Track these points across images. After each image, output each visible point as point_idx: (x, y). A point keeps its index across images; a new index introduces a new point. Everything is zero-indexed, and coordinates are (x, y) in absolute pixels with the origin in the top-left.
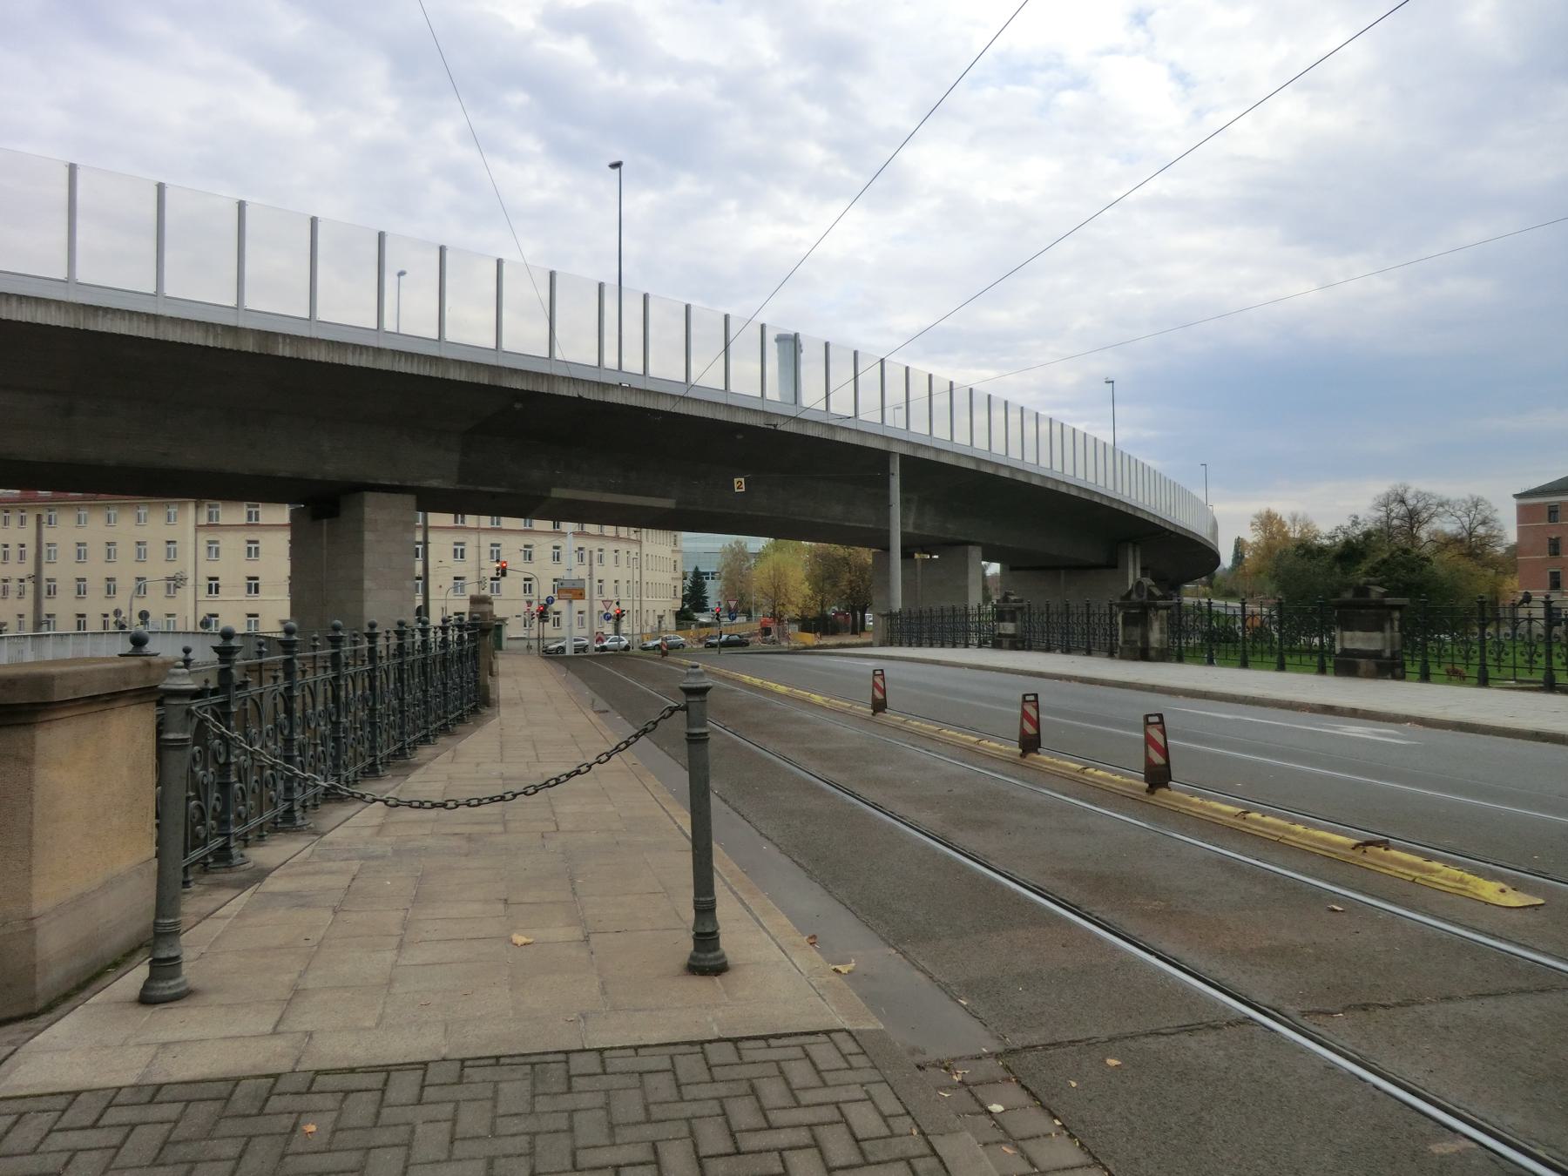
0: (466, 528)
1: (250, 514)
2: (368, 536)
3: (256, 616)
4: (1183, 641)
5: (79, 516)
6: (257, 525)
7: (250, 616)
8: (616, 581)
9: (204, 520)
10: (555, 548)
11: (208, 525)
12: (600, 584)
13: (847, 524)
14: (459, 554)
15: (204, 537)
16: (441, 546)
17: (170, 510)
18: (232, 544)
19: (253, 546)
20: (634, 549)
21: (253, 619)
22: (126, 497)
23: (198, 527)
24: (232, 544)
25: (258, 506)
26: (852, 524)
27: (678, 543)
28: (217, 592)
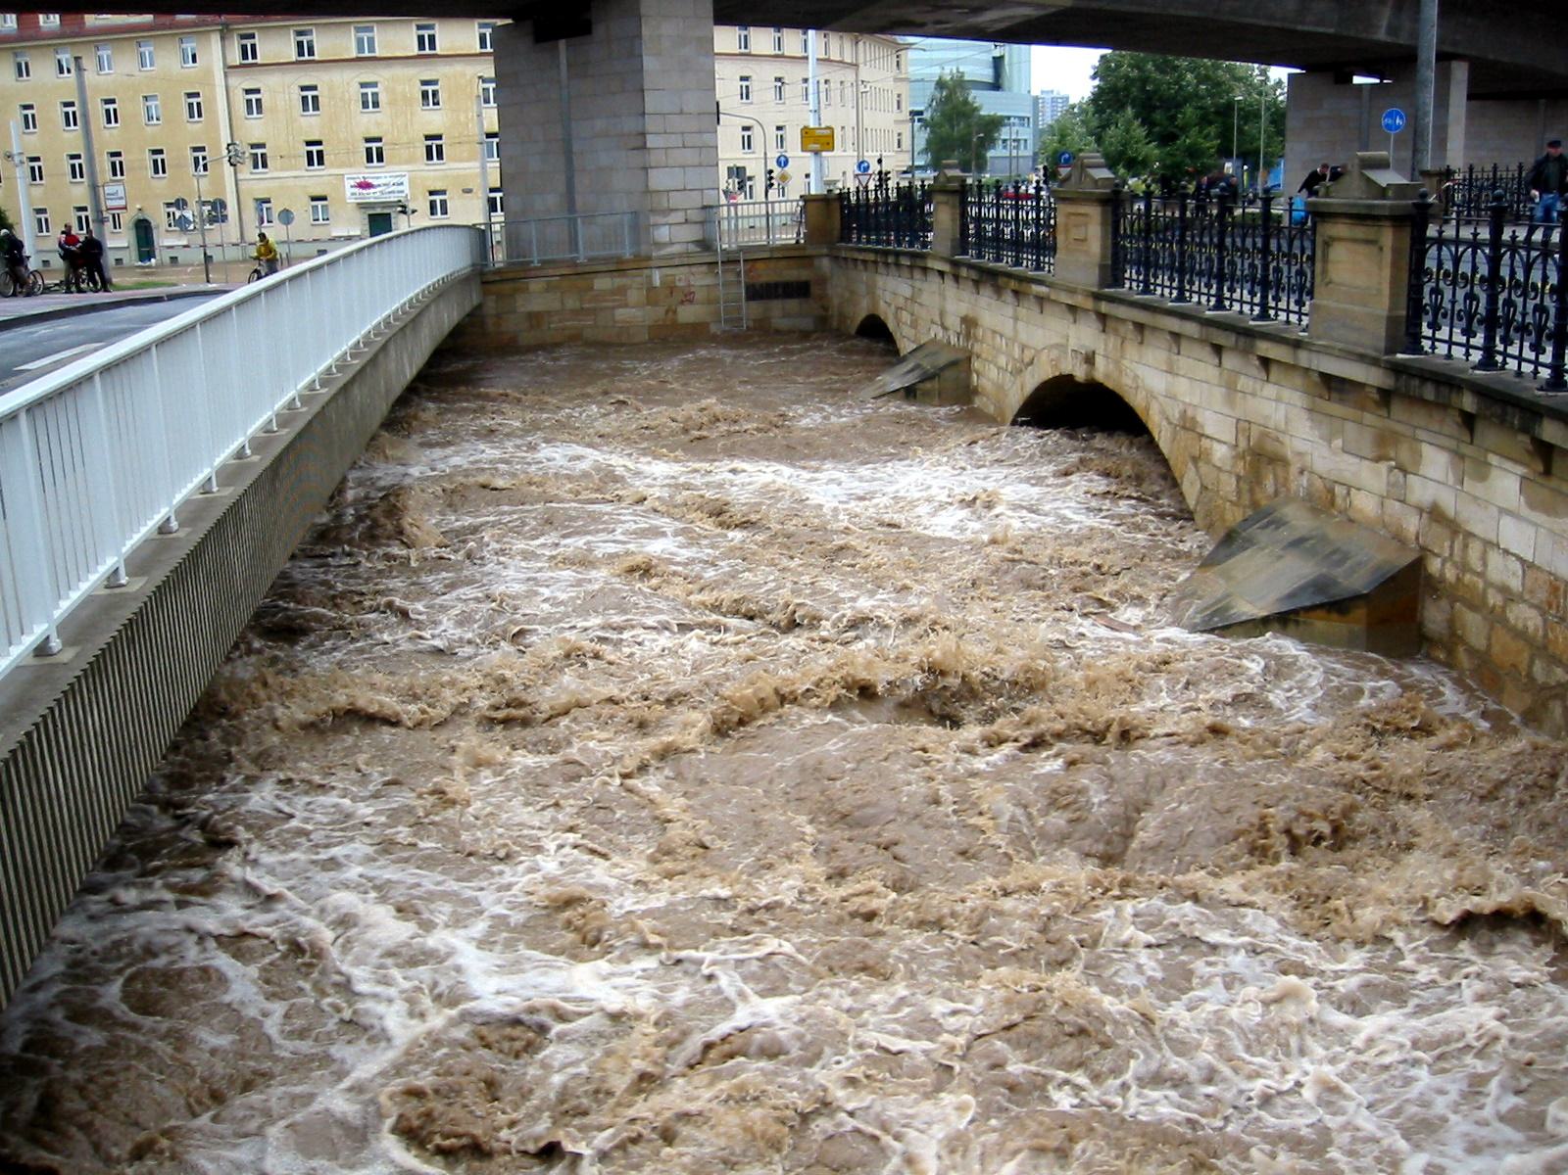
0: (782, 56)
1: (360, 42)
2: (649, 63)
3: (324, 198)
4: (1177, 215)
5: (142, 55)
6: (256, 65)
7: (314, 199)
8: (779, 128)
9: (235, 58)
10: (743, 79)
11: (297, 62)
12: (780, 133)
13: (1300, 27)
14: (310, 101)
15: (241, 82)
16: (726, 79)
17: (184, 46)
18: (280, 90)
19: (310, 94)
20: (849, 76)
21: (319, 204)
22: (257, 18)
23: (229, 68)
24: (280, 90)
25: (371, 30)
26: (1306, 28)
27: (902, 67)
28: (265, 165)
